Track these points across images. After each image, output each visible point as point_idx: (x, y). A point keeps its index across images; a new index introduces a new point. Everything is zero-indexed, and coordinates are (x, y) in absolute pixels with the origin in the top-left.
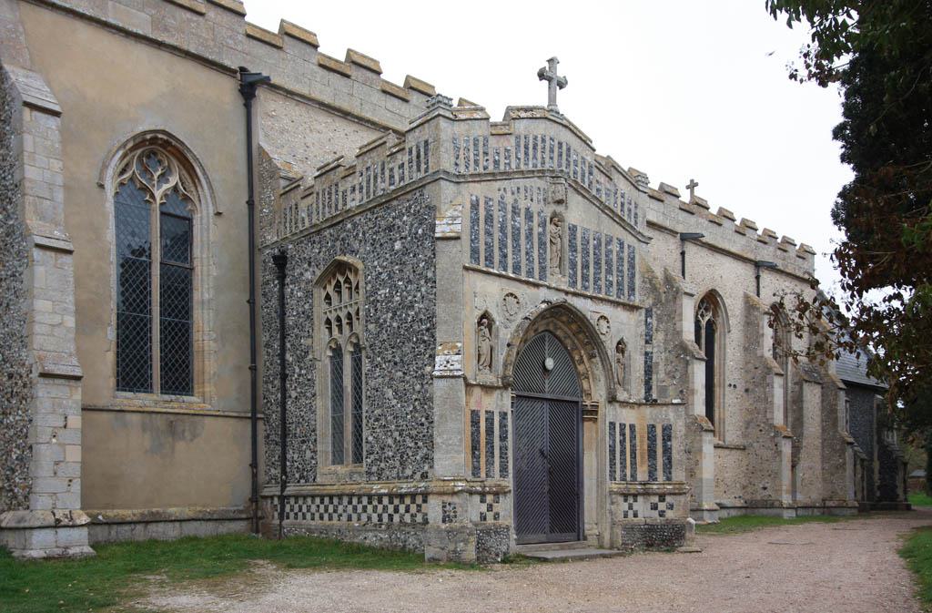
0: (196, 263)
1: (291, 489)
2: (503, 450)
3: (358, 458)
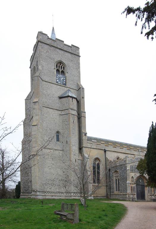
1: (111, 194)
2: (135, 190)
3: (119, 191)
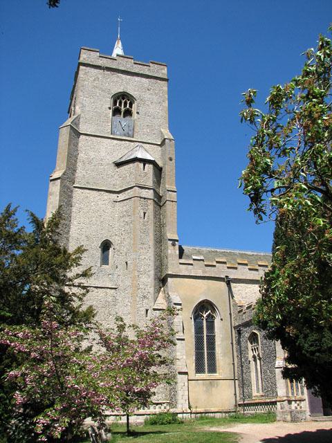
0: (216, 334)
